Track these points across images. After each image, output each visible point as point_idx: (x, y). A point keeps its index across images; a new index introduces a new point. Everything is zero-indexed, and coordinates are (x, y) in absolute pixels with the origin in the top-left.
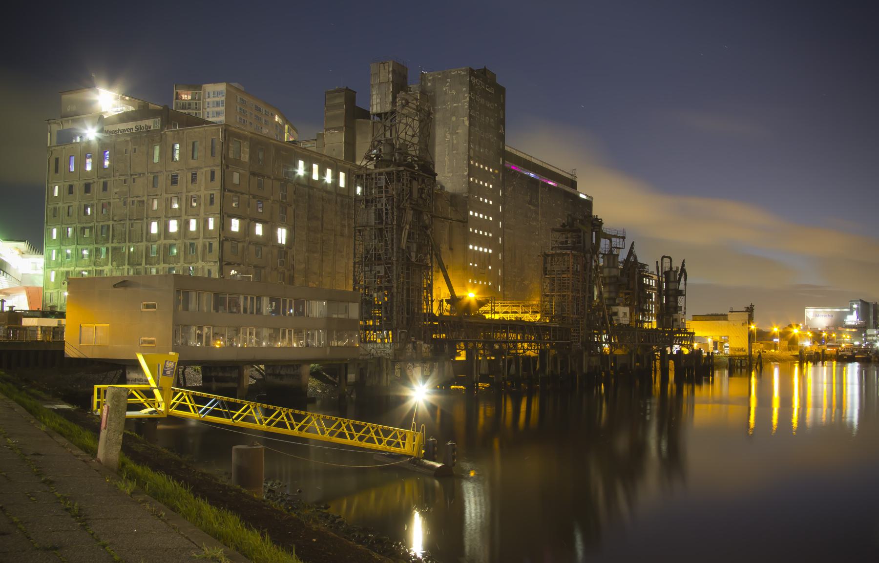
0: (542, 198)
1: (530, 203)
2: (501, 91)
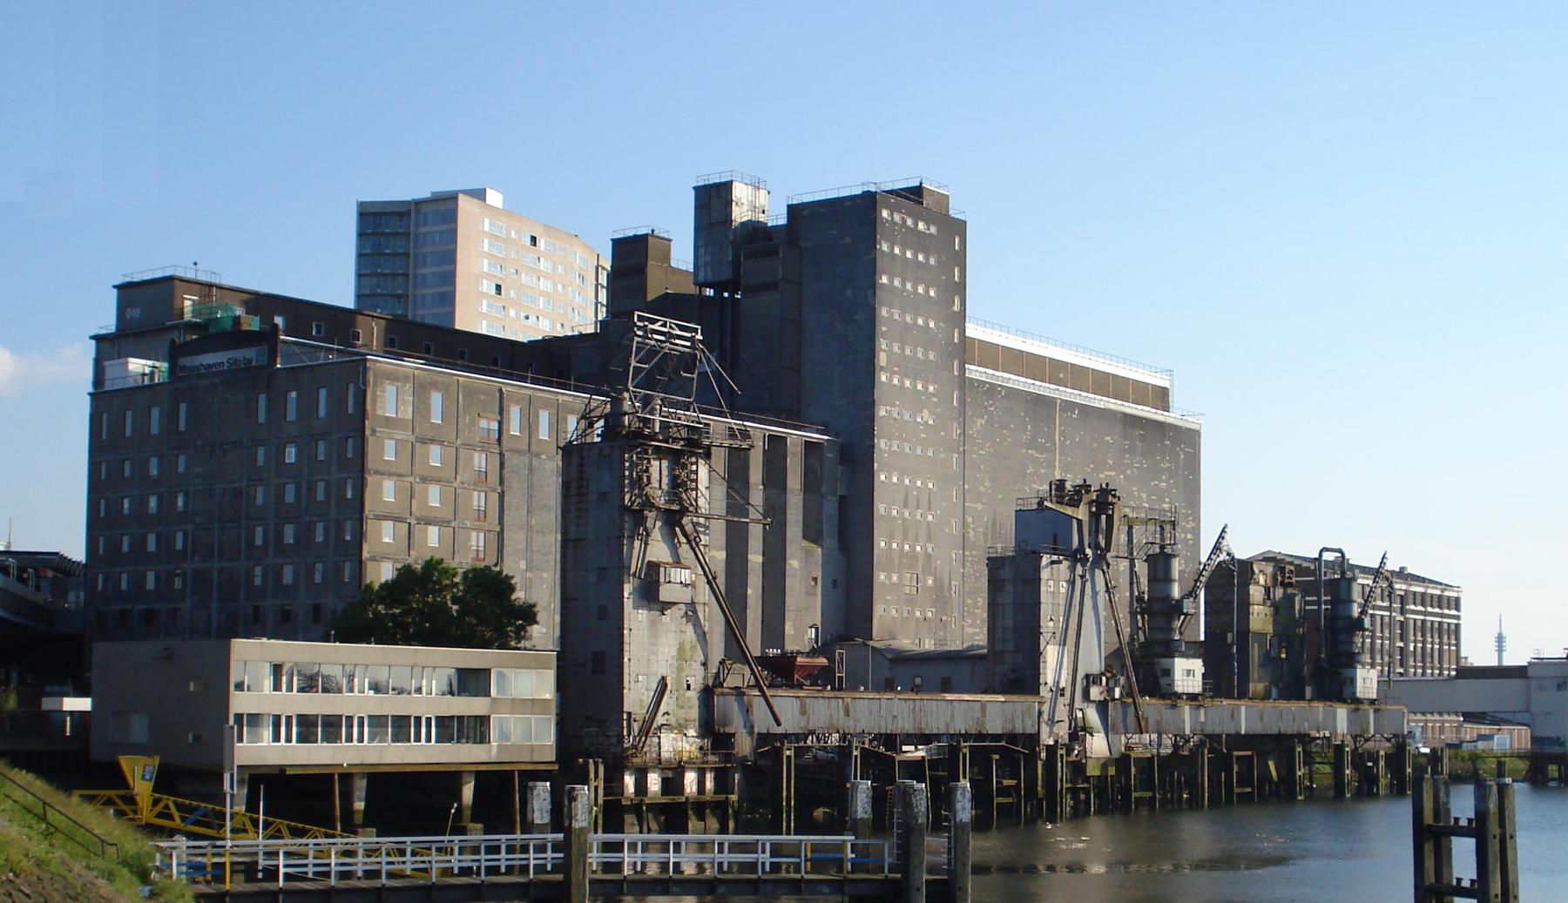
0: (1062, 433)
1: (1032, 444)
2: (960, 227)
